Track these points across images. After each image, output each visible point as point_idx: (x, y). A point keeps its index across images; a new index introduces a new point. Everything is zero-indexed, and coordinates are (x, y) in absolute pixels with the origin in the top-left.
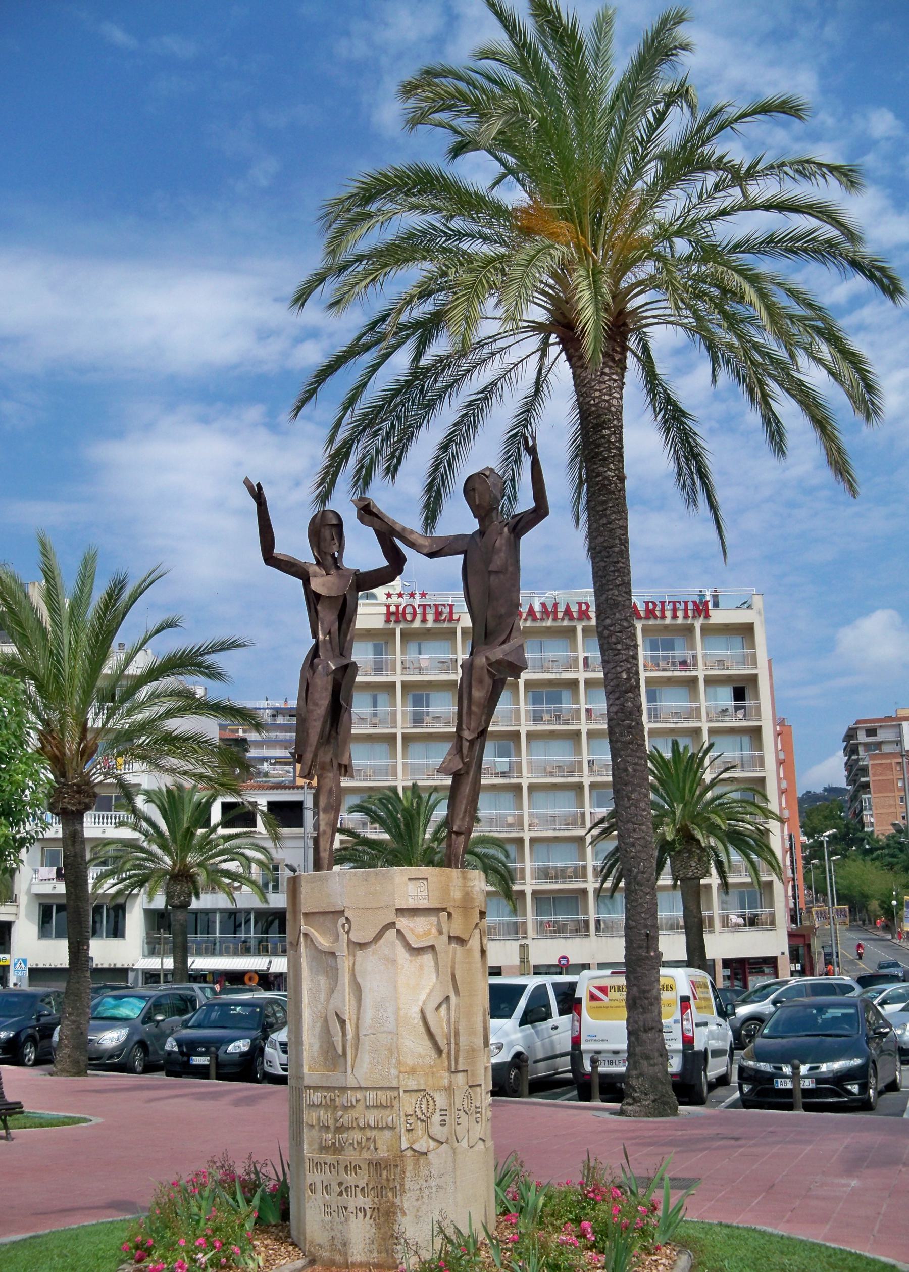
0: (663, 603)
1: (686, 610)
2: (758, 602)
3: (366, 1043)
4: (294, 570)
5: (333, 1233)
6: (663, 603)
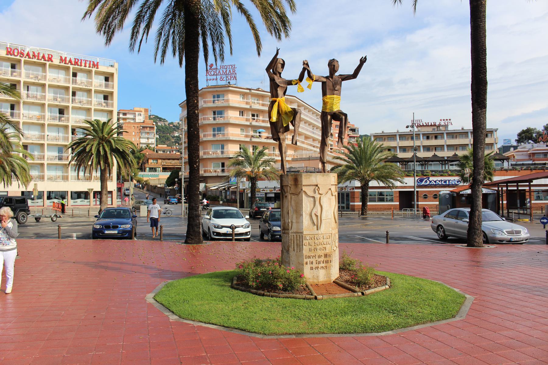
0: (81, 60)
1: (90, 64)
2: (116, 65)
6: (81, 60)
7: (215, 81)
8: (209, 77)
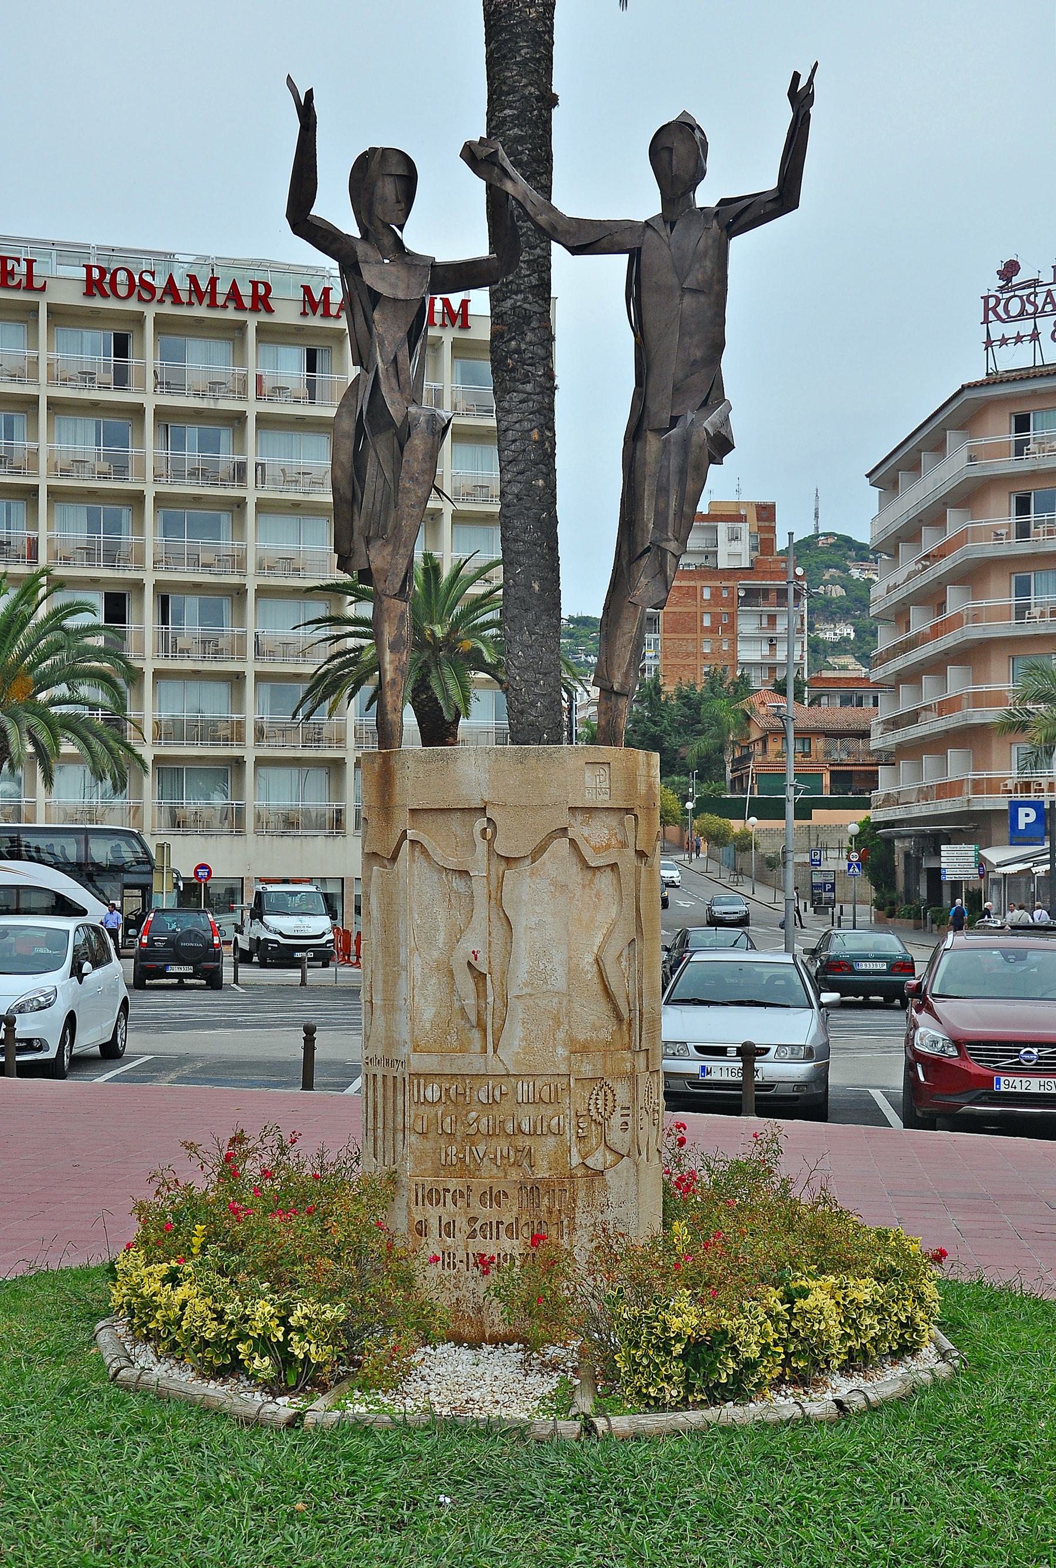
3: (518, 1011)
4: (334, 247)
5: (457, 1294)
7: (1027, 346)
8: (998, 330)
